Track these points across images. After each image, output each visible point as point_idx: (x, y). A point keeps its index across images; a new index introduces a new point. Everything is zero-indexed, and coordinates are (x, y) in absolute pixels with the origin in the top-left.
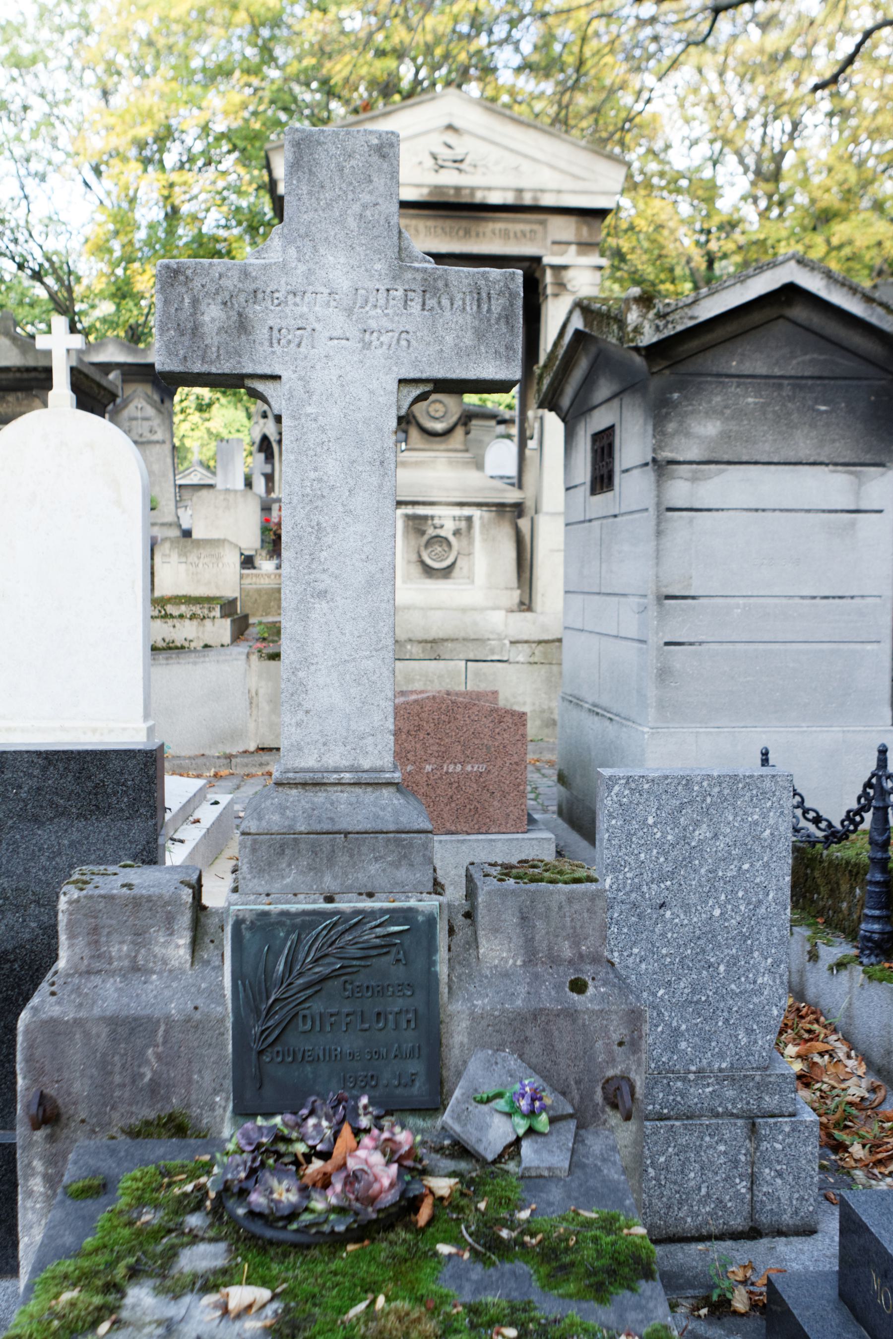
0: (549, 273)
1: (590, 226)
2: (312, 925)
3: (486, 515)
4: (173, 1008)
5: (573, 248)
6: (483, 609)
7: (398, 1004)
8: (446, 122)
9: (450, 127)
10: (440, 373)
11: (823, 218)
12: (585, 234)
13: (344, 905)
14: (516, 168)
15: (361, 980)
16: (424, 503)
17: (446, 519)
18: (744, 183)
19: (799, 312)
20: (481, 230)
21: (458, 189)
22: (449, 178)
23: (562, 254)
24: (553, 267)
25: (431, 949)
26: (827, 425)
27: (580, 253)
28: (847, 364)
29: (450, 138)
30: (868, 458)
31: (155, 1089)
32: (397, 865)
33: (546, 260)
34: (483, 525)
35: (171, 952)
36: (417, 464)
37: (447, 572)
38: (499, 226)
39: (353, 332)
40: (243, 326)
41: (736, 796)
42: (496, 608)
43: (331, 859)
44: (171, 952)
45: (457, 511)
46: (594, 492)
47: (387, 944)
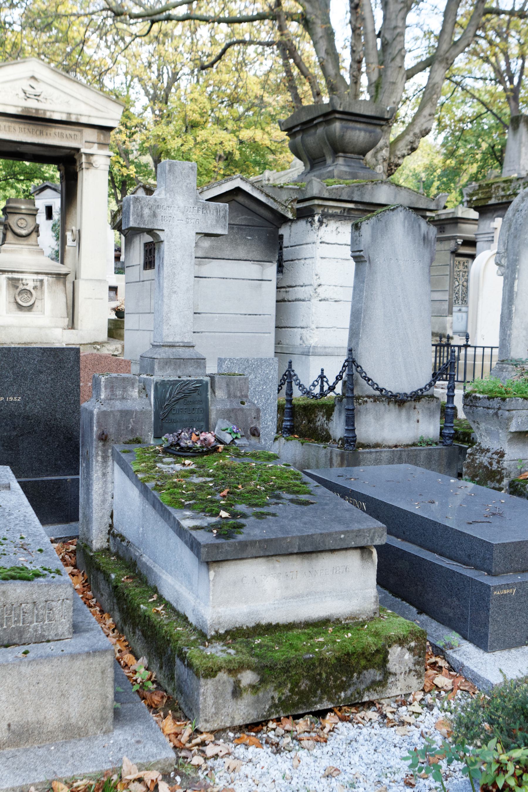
0: (84, 156)
1: (104, 135)
2: (176, 384)
3: (51, 279)
4: (137, 408)
5: (96, 145)
6: (50, 328)
7: (198, 406)
8: (31, 74)
9: (33, 78)
10: (207, 231)
11: (192, 126)
12: (102, 138)
13: (185, 378)
14: (67, 102)
15: (189, 399)
16: (22, 272)
17: (30, 281)
18: (145, 100)
19: (241, 199)
20: (49, 132)
21: (37, 110)
22: (32, 104)
23: (90, 148)
24: (85, 154)
25: (207, 391)
26: (251, 245)
27: (99, 148)
28: (258, 220)
29: (33, 83)
30: (266, 259)
31: (132, 431)
32: (196, 368)
33: (82, 150)
34: (49, 284)
35: (133, 393)
36: (12, 251)
37: (30, 308)
38: (58, 131)
39: (184, 219)
40: (154, 215)
41: (262, 365)
42: (57, 327)
43: (179, 366)
44: (133, 393)
45: (35, 277)
46: (145, 268)
47: (196, 389)
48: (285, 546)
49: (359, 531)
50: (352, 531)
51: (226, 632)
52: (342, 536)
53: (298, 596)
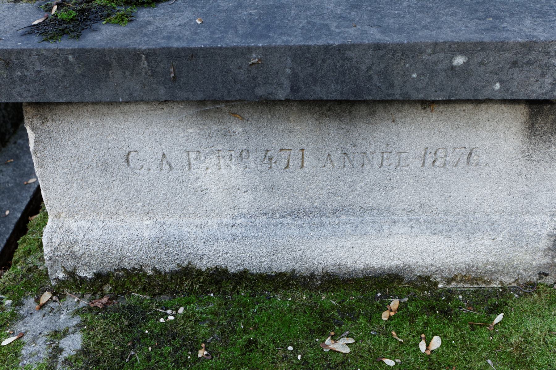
48: (242, 75)
49: (529, 46)
50: (501, 47)
51: (98, 276)
52: (459, 60)
53: (307, 213)
